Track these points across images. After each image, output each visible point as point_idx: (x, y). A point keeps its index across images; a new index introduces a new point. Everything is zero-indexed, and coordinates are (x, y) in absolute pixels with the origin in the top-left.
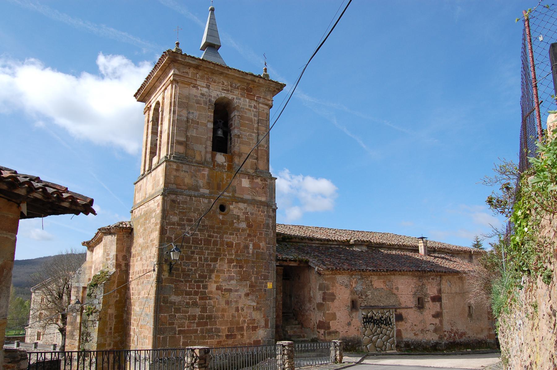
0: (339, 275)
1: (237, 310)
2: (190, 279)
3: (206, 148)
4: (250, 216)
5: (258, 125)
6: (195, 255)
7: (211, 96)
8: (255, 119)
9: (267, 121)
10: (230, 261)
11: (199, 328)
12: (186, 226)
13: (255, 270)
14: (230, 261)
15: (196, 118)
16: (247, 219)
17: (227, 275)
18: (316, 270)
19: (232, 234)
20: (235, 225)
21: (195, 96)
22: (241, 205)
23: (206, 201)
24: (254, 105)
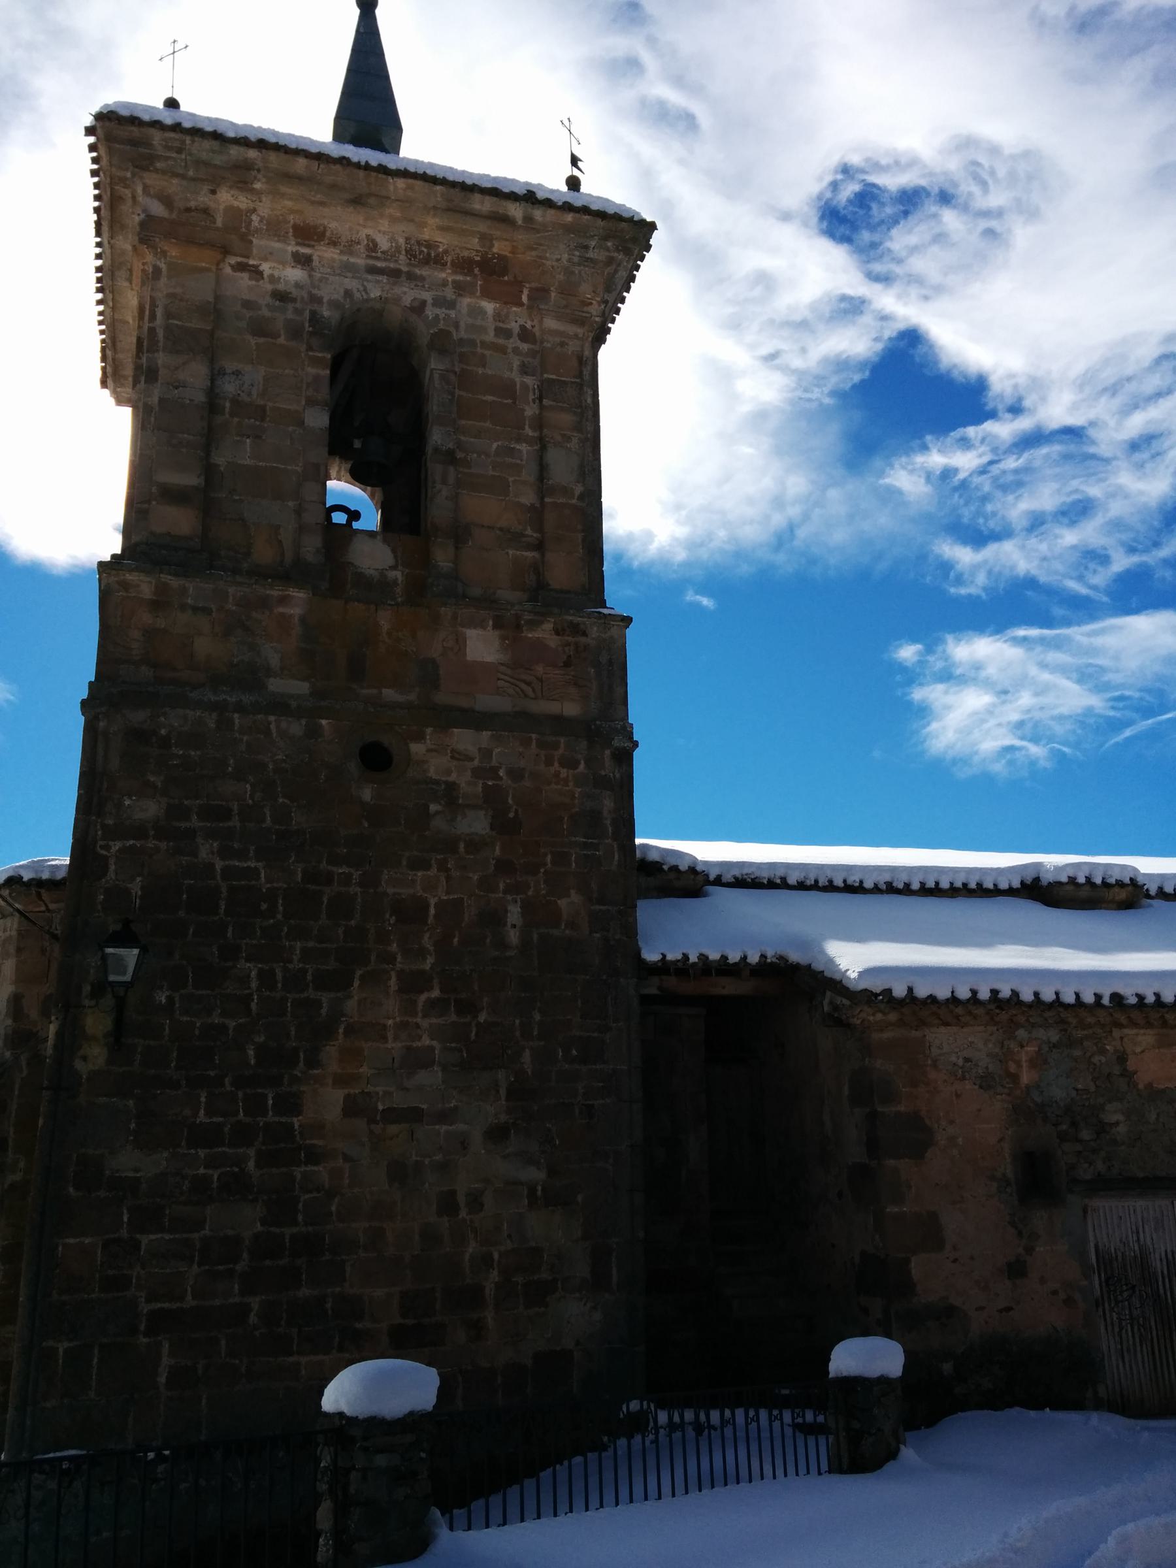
0: (943, 1029)
1: (448, 1204)
2: (212, 1073)
3: (299, 512)
4: (506, 781)
5: (542, 407)
6: (243, 964)
7: (319, 300)
8: (525, 387)
9: (580, 386)
10: (413, 983)
11: (255, 1302)
12: (199, 840)
13: (537, 1017)
14: (413, 983)
15: (254, 392)
16: (492, 798)
17: (395, 1046)
18: (826, 1008)
19: (416, 865)
20: (438, 823)
21: (248, 304)
22: (465, 739)
23: (296, 728)
24: (523, 328)
